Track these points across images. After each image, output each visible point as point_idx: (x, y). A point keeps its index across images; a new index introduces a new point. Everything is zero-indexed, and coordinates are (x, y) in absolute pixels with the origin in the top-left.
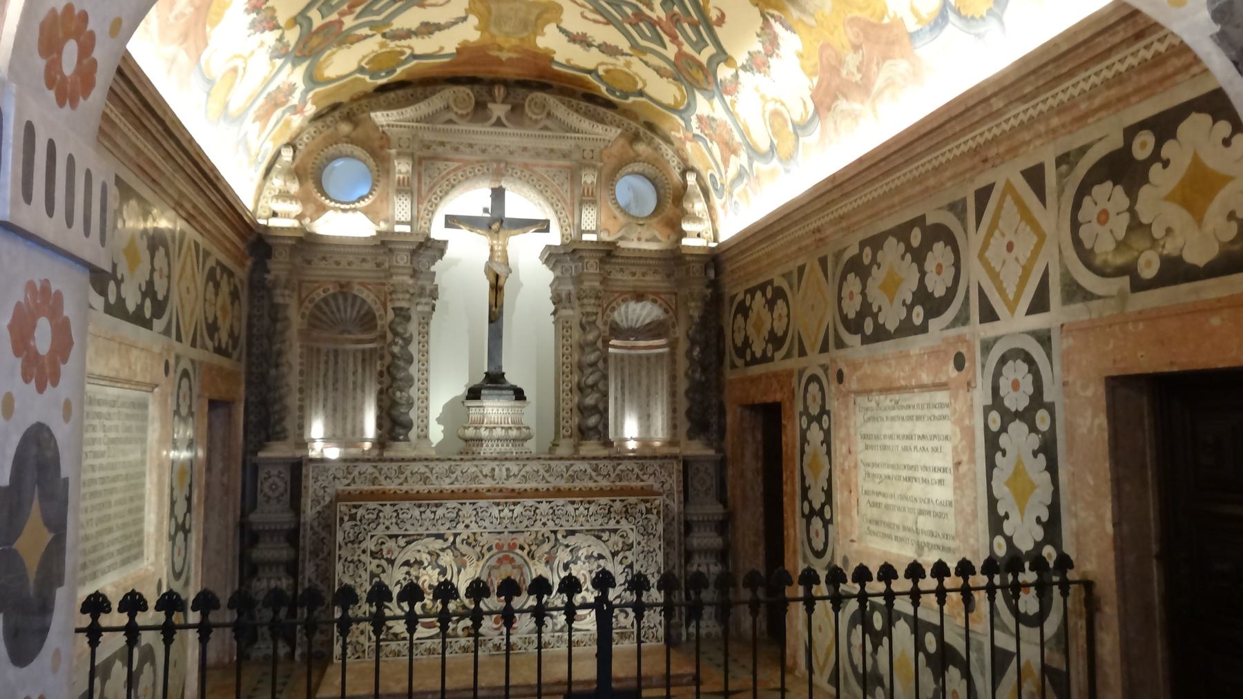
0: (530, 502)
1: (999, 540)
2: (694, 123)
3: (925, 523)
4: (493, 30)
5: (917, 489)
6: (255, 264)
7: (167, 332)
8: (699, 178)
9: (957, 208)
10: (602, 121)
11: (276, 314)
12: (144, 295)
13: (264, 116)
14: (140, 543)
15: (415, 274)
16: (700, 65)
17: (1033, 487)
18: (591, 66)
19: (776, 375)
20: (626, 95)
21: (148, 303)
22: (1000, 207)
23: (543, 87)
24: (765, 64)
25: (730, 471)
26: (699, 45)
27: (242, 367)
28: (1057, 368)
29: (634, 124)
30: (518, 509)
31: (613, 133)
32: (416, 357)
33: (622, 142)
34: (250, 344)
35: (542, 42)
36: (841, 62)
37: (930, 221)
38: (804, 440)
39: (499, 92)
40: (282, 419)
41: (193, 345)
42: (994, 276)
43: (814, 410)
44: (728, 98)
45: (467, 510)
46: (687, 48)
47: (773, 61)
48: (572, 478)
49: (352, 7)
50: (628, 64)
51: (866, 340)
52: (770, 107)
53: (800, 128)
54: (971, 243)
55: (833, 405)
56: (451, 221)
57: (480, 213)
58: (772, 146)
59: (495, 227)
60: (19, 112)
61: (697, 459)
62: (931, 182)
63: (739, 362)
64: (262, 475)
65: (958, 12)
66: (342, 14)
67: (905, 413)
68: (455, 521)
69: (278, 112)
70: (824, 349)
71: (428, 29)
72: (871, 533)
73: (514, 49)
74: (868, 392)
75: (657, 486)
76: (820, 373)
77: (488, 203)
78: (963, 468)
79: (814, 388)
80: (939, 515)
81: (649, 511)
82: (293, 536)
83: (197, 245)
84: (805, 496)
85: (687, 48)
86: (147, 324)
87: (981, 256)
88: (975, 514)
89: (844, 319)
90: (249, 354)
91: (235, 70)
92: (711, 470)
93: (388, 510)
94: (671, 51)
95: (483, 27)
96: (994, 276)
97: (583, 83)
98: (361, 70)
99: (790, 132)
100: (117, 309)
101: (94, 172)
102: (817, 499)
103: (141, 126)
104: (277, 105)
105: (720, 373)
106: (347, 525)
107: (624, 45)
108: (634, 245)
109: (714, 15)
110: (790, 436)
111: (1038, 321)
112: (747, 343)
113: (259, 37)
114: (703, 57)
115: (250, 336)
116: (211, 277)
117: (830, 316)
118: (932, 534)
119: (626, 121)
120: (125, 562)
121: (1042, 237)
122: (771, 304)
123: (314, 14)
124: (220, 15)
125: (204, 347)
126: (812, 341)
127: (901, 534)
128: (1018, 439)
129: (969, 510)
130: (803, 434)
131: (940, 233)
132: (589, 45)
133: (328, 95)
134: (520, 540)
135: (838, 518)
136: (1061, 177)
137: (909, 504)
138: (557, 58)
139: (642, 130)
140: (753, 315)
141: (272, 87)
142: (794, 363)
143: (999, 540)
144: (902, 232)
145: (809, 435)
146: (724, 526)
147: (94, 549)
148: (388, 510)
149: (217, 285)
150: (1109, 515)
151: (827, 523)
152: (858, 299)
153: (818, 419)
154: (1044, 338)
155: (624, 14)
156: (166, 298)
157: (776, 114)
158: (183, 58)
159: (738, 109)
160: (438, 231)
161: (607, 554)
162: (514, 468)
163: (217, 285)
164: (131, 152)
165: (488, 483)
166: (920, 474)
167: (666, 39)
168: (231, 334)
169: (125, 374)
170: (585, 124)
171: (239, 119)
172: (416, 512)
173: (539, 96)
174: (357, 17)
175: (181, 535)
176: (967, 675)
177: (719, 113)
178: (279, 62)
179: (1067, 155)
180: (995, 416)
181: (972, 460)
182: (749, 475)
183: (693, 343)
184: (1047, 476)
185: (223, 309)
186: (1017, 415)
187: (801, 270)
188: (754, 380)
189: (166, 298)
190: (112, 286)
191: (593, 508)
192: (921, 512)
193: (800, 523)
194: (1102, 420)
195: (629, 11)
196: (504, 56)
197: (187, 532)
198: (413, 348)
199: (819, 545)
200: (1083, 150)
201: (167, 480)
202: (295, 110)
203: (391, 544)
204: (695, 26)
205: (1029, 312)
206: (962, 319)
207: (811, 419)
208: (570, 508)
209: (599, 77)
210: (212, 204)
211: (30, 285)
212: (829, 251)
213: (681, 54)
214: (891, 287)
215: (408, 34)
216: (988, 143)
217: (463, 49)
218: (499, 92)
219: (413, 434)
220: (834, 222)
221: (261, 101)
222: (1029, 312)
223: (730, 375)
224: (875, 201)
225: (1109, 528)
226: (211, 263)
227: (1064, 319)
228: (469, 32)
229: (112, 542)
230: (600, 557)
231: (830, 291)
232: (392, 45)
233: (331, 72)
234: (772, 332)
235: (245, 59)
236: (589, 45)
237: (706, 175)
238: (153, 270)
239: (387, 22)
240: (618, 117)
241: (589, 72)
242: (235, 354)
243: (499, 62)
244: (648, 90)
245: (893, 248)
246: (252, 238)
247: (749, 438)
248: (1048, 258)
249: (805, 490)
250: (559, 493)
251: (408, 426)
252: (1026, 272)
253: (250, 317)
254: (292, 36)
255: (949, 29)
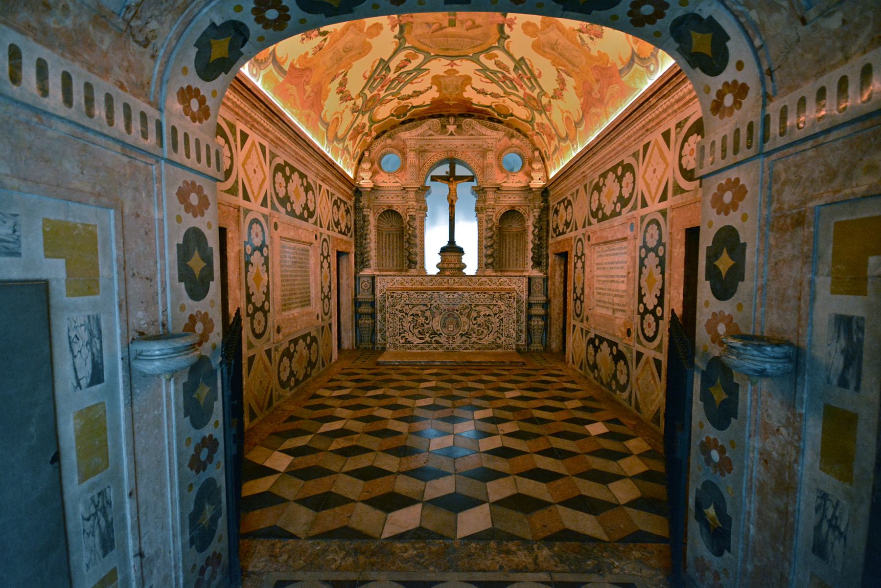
0: (460, 293)
1: (641, 305)
2: (536, 127)
3: (617, 300)
4: (444, 92)
5: (614, 286)
6: (356, 199)
7: (315, 223)
8: (540, 153)
9: (635, 155)
10: (497, 130)
11: (365, 219)
12: (304, 209)
13: (353, 138)
14: (309, 300)
15: (417, 201)
16: (534, 99)
17: (655, 280)
18: (489, 104)
19: (567, 239)
20: (506, 117)
21: (306, 212)
22: (652, 152)
23: (470, 116)
24: (561, 94)
25: (549, 283)
26: (532, 88)
27: (352, 240)
28: (668, 226)
29: (511, 130)
30: (456, 295)
31: (501, 134)
32: (418, 235)
33: (506, 138)
34: (355, 231)
35: (466, 95)
36: (592, 90)
37: (625, 163)
38: (575, 267)
39: (452, 120)
40: (368, 260)
41: (328, 229)
42: (647, 185)
43: (579, 255)
44: (548, 113)
45: (436, 295)
46: (528, 91)
47: (564, 93)
48: (480, 284)
49: (382, 87)
50: (504, 101)
51: (599, 221)
52: (565, 115)
53: (577, 124)
54: (640, 171)
55: (586, 251)
56: (434, 179)
57: (445, 174)
58: (567, 134)
59: (451, 179)
60: (168, 122)
61: (536, 277)
62: (626, 143)
63: (554, 235)
64: (361, 281)
65: (638, 57)
66: (379, 91)
67: (611, 252)
68: (431, 299)
69: (360, 136)
70: (584, 227)
71: (417, 94)
72: (597, 305)
73: (454, 99)
74: (598, 244)
75: (516, 288)
76: (582, 237)
77: (448, 170)
78: (630, 275)
79: (580, 243)
80: (622, 296)
81: (510, 297)
82: (373, 304)
83: (328, 191)
84: (575, 292)
85: (528, 91)
86: (306, 220)
87: (643, 177)
88: (633, 295)
89: (592, 211)
90: (356, 235)
91: (337, 118)
92: (541, 282)
93: (405, 294)
94: (521, 93)
95: (439, 91)
96: (647, 185)
97: (487, 113)
98: (392, 115)
99: (576, 125)
100: (292, 213)
101: (211, 146)
102: (579, 291)
103: (297, 143)
104: (359, 133)
105: (547, 240)
106: (390, 299)
107: (501, 92)
108: (511, 185)
109: (536, 73)
110: (570, 267)
111: (663, 205)
112: (557, 227)
113: (345, 104)
114: (535, 94)
115: (356, 228)
116: (335, 203)
117: (586, 212)
118: (619, 305)
119: (508, 129)
120: (302, 306)
121: (667, 164)
122: (566, 208)
123: (366, 91)
124: (327, 96)
125: (333, 230)
126: (580, 225)
127: (608, 305)
128: (652, 260)
129: (631, 293)
130: (575, 264)
131: (628, 168)
132: (486, 94)
133: (380, 128)
134: (457, 307)
135: (586, 300)
136: (677, 134)
137: (611, 292)
138: (474, 101)
139: (515, 132)
140: (560, 213)
141: (355, 125)
142: (573, 234)
143: (641, 305)
144: (614, 169)
145: (577, 265)
146: (546, 305)
147: (289, 299)
148: (405, 294)
149: (338, 207)
150: (682, 292)
151: (582, 302)
152: (597, 202)
153: (580, 258)
154: (664, 213)
155: (498, 77)
156: (314, 211)
157: (568, 118)
158: (312, 114)
159: (552, 118)
160: (428, 183)
161: (492, 314)
162: (457, 280)
163: (338, 207)
164: (293, 154)
165: (446, 286)
166: (616, 279)
167: (518, 87)
168: (347, 227)
169: (297, 238)
170: (489, 132)
171: (342, 140)
172: (416, 295)
173: (468, 120)
174: (251, 408)
175: (326, 300)
176: (626, 363)
177: (546, 121)
178: (356, 114)
179: (680, 123)
180: (643, 250)
181: (634, 272)
182: (557, 284)
183: (535, 227)
184: (660, 276)
185: (342, 216)
186: (652, 250)
187: (577, 191)
188: (559, 243)
189: (314, 211)
190: (288, 204)
191: (486, 296)
192: (615, 296)
193: (572, 302)
194: (683, 249)
195: (500, 76)
196: (451, 103)
197: (329, 299)
198: (417, 232)
199: (578, 312)
200: (686, 120)
201: (319, 278)
202: (367, 134)
203: (407, 307)
204: (529, 79)
205: (660, 202)
206: (634, 208)
207: (579, 258)
208: (477, 295)
209: (493, 109)
210: (334, 175)
211: (185, 182)
212: (587, 181)
213: (525, 94)
214: (608, 196)
215: (409, 97)
216: (647, 123)
217: (434, 102)
218: (452, 120)
219: (418, 266)
220: (590, 168)
221: (351, 132)
222: (660, 202)
223: (551, 241)
224: (604, 157)
225: (682, 298)
226: (335, 198)
227: (672, 204)
228: (434, 94)
229: (296, 298)
230: (489, 315)
231: (587, 199)
232: (403, 102)
233: (379, 117)
234: (566, 221)
235: (341, 114)
236: (486, 94)
237: (543, 151)
238: (307, 200)
239: (398, 92)
240: (504, 127)
241: (488, 107)
242: (349, 235)
243: (449, 106)
244: (514, 113)
245: (611, 176)
246: (354, 189)
247: (558, 268)
248: (669, 175)
249: (575, 288)
250: (474, 289)
251: (416, 263)
252: (660, 181)
253: (355, 221)
254: (360, 102)
255: (636, 66)
